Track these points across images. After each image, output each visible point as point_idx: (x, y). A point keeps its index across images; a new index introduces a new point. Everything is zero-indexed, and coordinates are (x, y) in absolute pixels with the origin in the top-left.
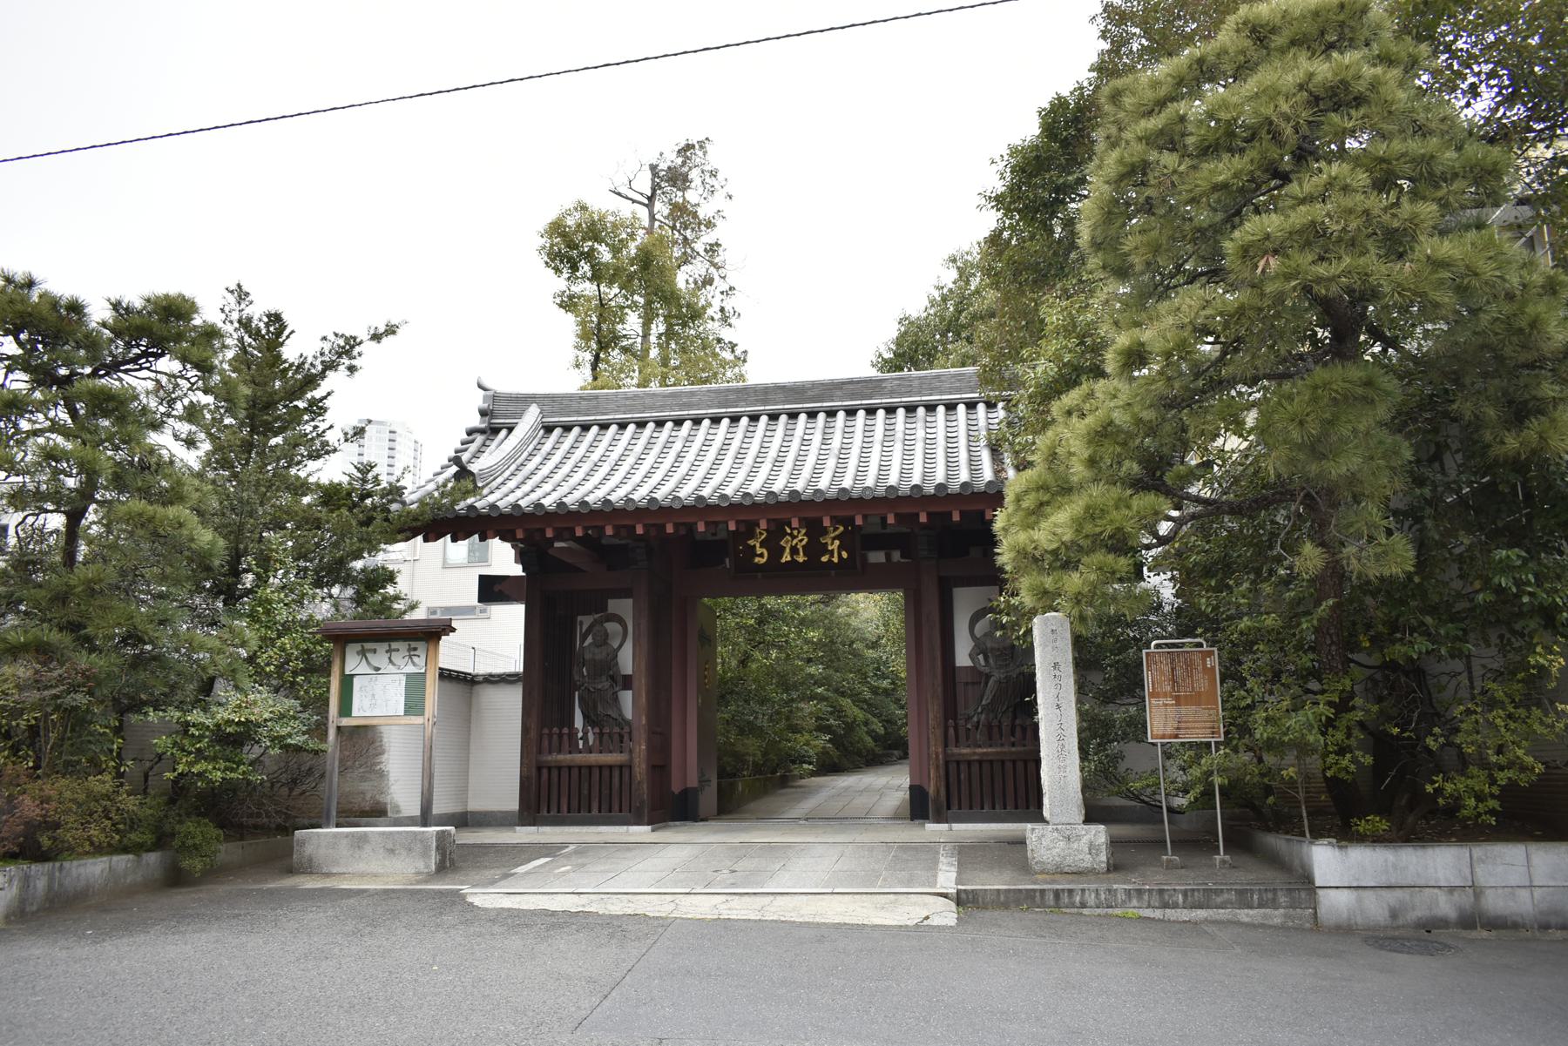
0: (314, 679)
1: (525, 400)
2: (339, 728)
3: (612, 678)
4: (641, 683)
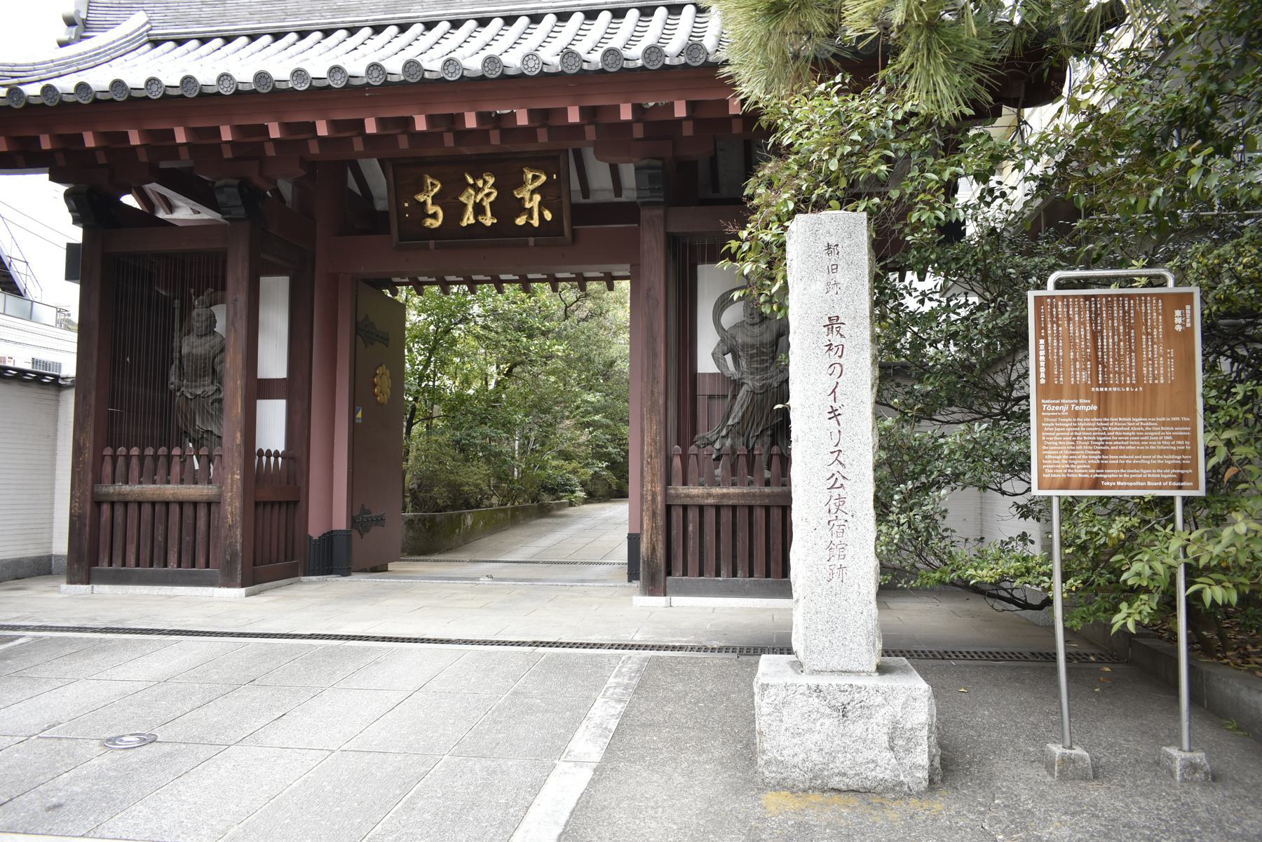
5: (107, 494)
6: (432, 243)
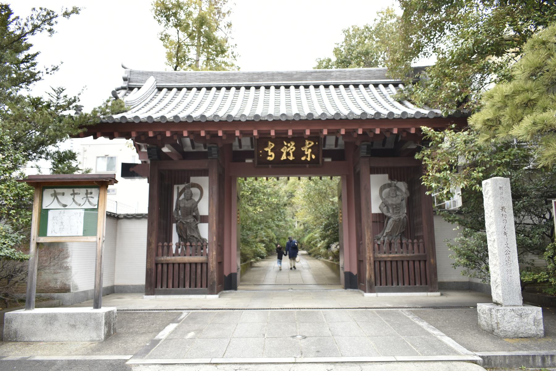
0: (23, 212)
1: (147, 74)
2: (38, 244)
3: (194, 217)
4: (214, 219)
5: (161, 260)
6: (270, 166)
